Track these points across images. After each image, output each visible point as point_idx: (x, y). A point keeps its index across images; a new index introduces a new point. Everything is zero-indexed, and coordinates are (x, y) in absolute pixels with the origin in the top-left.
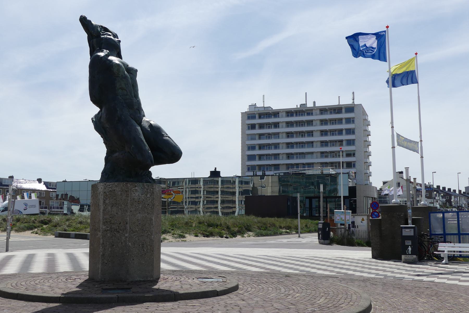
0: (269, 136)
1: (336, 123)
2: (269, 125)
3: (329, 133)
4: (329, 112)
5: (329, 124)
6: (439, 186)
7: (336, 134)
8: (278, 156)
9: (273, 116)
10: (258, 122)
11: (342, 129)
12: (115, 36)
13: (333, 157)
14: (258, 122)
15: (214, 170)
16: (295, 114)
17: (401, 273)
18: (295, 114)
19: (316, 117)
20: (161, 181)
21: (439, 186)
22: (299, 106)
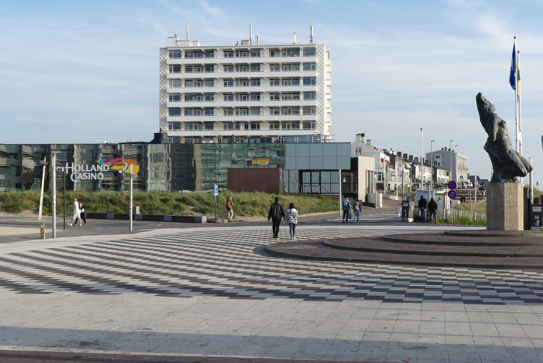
0: (199, 82)
1: (290, 69)
2: (199, 68)
3: (281, 82)
4: (281, 54)
5: (281, 69)
6: (412, 156)
7: (290, 84)
8: (211, 111)
9: (204, 55)
10: (189, 62)
11: (299, 77)
12: (519, 79)
13: (286, 114)
14: (189, 62)
15: (158, 132)
16: (235, 54)
17: (316, 266)
18: (235, 54)
19: (265, 58)
20: (391, 200)
21: (412, 156)
22: (240, 44)
